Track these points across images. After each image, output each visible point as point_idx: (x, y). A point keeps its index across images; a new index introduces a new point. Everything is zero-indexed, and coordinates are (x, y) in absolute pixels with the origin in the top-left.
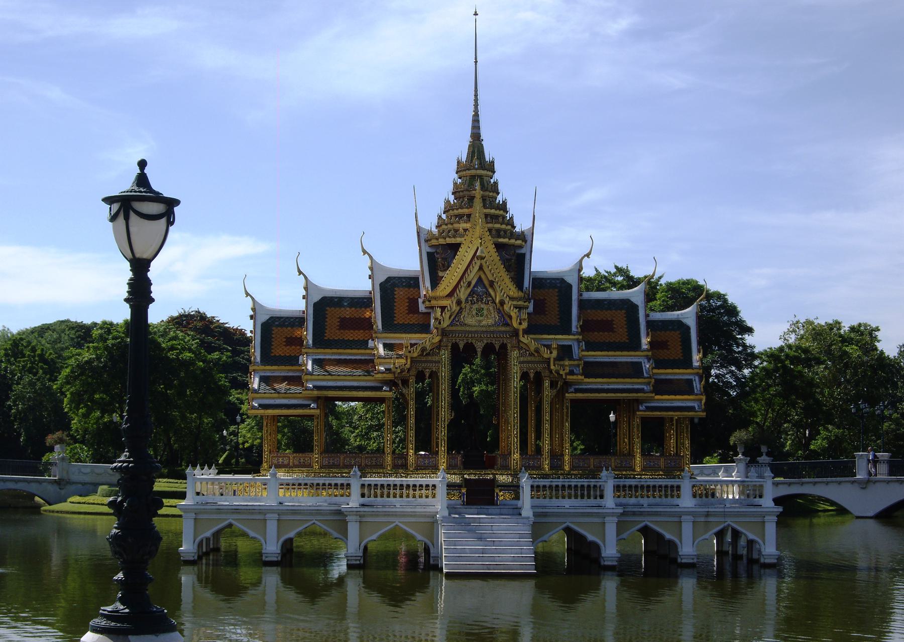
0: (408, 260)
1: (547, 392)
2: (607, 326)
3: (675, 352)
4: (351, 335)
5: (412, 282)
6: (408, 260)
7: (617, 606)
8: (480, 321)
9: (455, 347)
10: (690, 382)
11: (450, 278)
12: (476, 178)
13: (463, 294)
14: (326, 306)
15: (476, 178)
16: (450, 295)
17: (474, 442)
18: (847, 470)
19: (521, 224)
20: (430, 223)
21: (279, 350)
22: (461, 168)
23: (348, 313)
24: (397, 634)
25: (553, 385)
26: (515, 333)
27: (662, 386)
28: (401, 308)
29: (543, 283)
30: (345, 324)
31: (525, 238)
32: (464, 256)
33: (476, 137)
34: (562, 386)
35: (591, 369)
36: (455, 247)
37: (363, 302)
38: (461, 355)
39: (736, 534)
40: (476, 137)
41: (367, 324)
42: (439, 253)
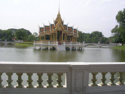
0: (53, 23)
1: (65, 35)
2: (70, 29)
3: (65, 28)
4: (48, 29)
5: (53, 25)
6: (53, 23)
7: (1, 77)
8: (60, 29)
9: (58, 31)
10: (73, 33)
11: (57, 25)
12: (59, 16)
13: (58, 26)
14: (46, 27)
15: (59, 16)
16: (57, 26)
17: (59, 39)
18: (5, 41)
19: (63, 20)
20: (55, 20)
21: (41, 30)
22: (58, 15)
23: (48, 27)
24: (99, 39)
25: (66, 34)
26: (63, 30)
27: (75, 35)
28: (52, 27)
29: (64, 25)
30: (47, 28)
31: (63, 21)
32: (58, 23)
33: (59, 12)
34: (67, 34)
35: (69, 33)
36: (57, 22)
37: (49, 26)
38: (58, 31)
39: (68, 48)
40: (59, 12)
41: (49, 29)
42: (56, 22)
